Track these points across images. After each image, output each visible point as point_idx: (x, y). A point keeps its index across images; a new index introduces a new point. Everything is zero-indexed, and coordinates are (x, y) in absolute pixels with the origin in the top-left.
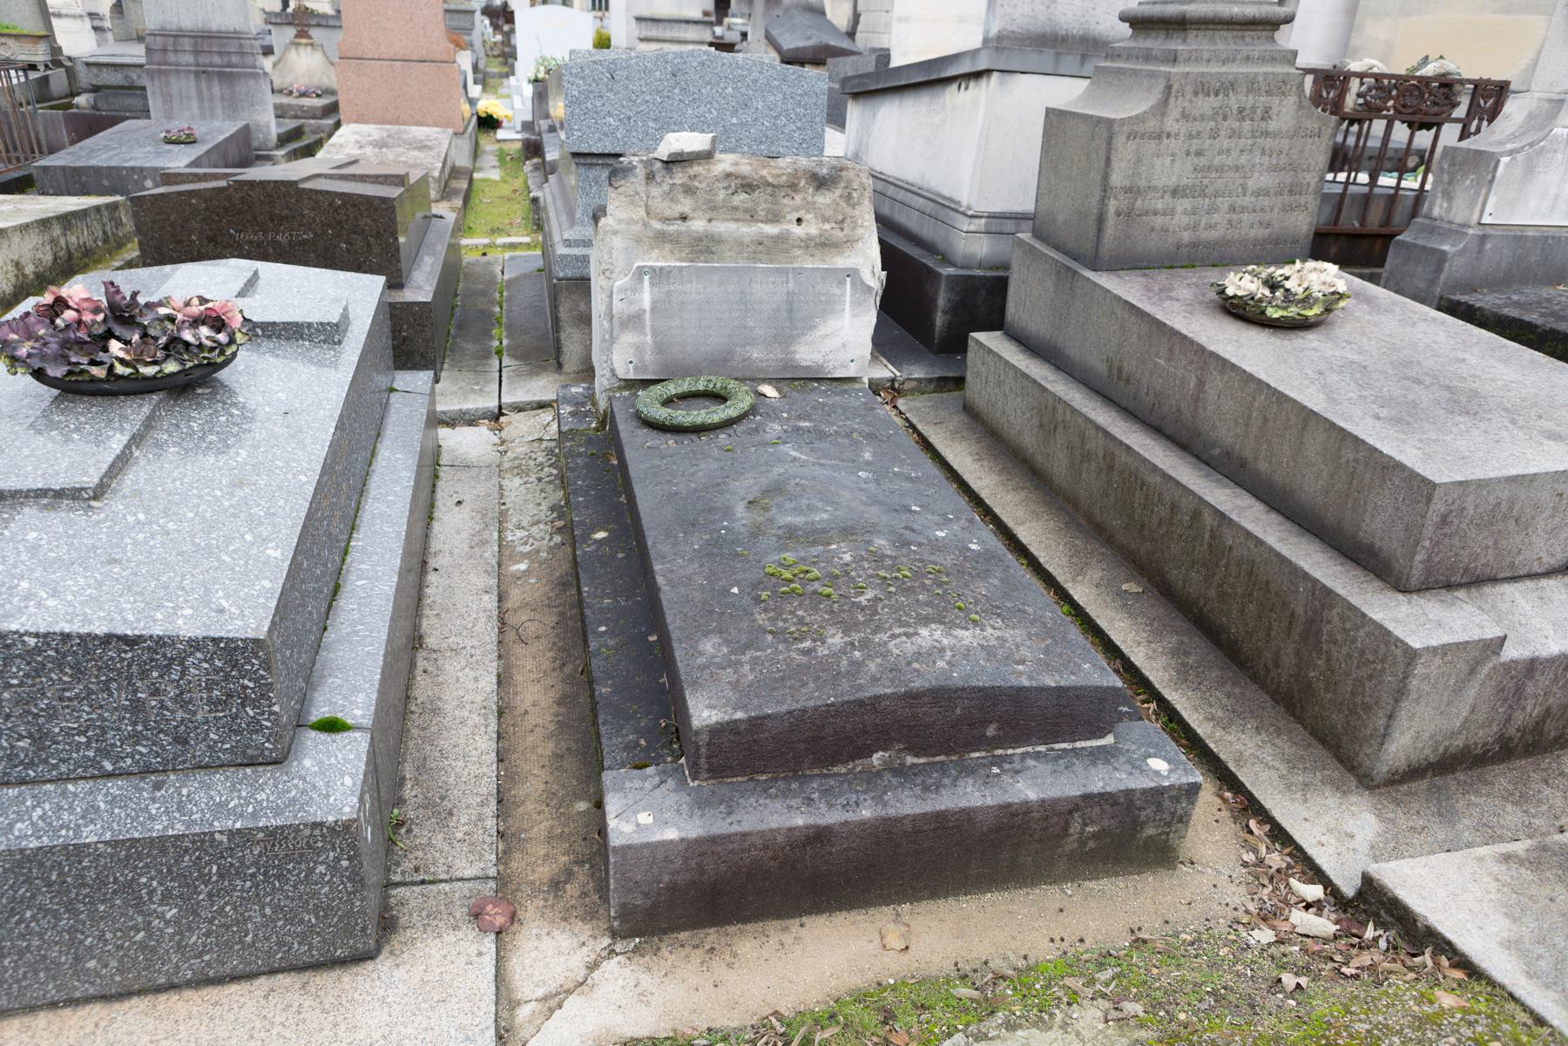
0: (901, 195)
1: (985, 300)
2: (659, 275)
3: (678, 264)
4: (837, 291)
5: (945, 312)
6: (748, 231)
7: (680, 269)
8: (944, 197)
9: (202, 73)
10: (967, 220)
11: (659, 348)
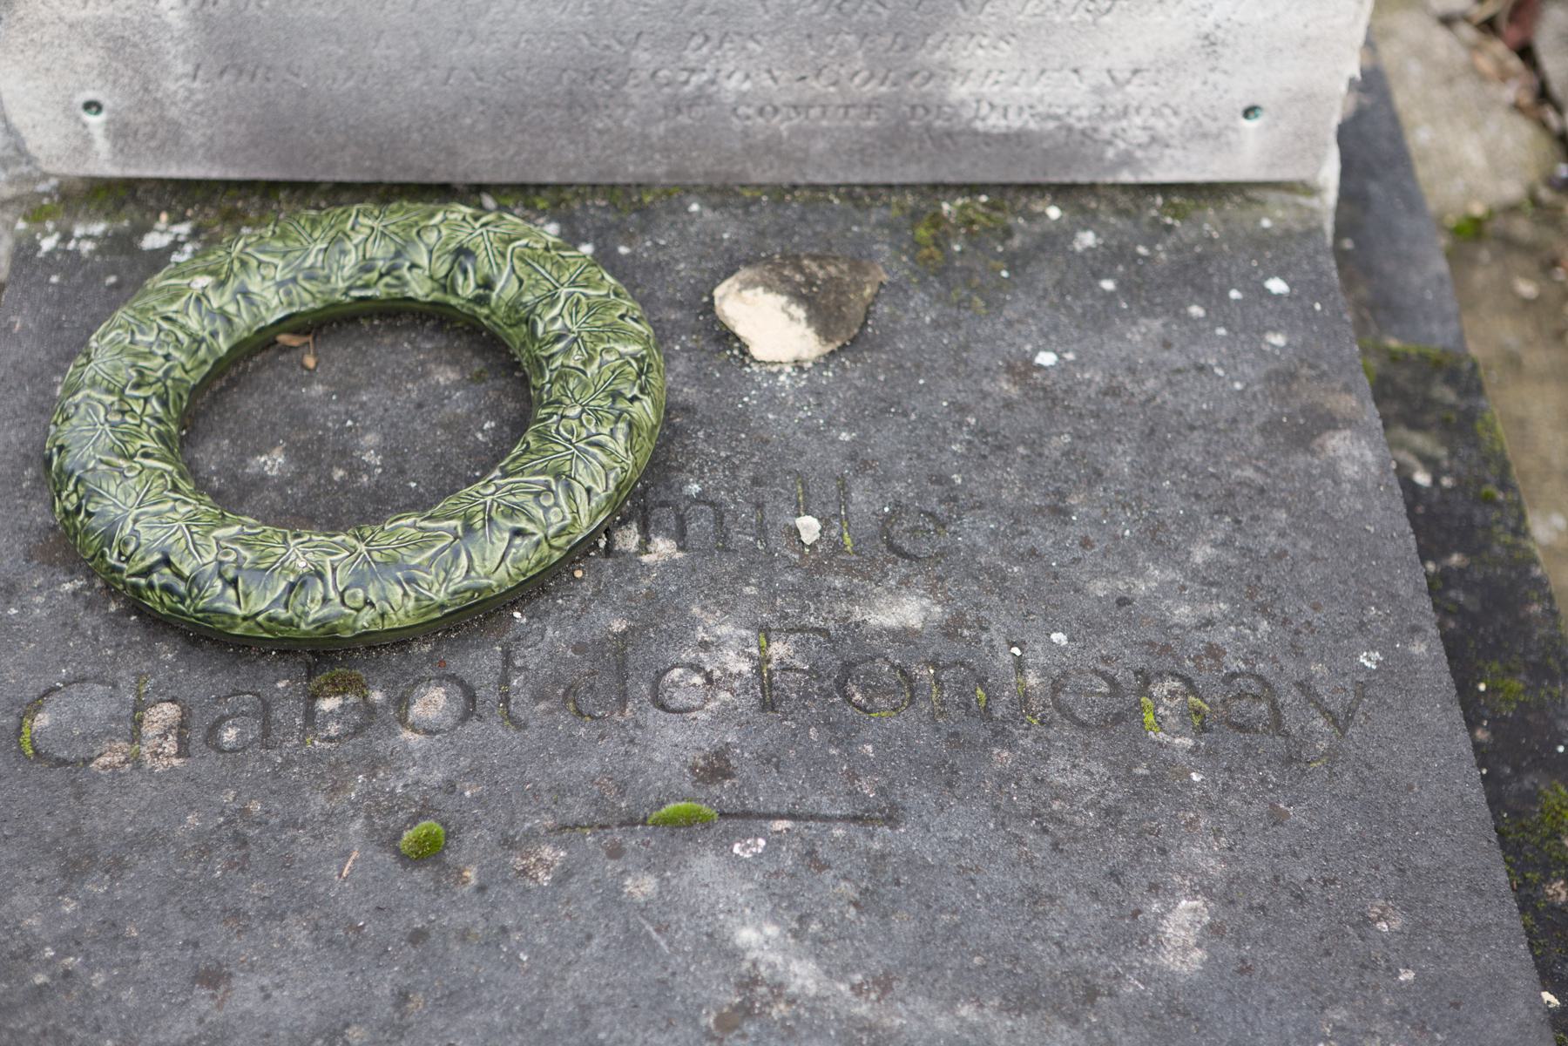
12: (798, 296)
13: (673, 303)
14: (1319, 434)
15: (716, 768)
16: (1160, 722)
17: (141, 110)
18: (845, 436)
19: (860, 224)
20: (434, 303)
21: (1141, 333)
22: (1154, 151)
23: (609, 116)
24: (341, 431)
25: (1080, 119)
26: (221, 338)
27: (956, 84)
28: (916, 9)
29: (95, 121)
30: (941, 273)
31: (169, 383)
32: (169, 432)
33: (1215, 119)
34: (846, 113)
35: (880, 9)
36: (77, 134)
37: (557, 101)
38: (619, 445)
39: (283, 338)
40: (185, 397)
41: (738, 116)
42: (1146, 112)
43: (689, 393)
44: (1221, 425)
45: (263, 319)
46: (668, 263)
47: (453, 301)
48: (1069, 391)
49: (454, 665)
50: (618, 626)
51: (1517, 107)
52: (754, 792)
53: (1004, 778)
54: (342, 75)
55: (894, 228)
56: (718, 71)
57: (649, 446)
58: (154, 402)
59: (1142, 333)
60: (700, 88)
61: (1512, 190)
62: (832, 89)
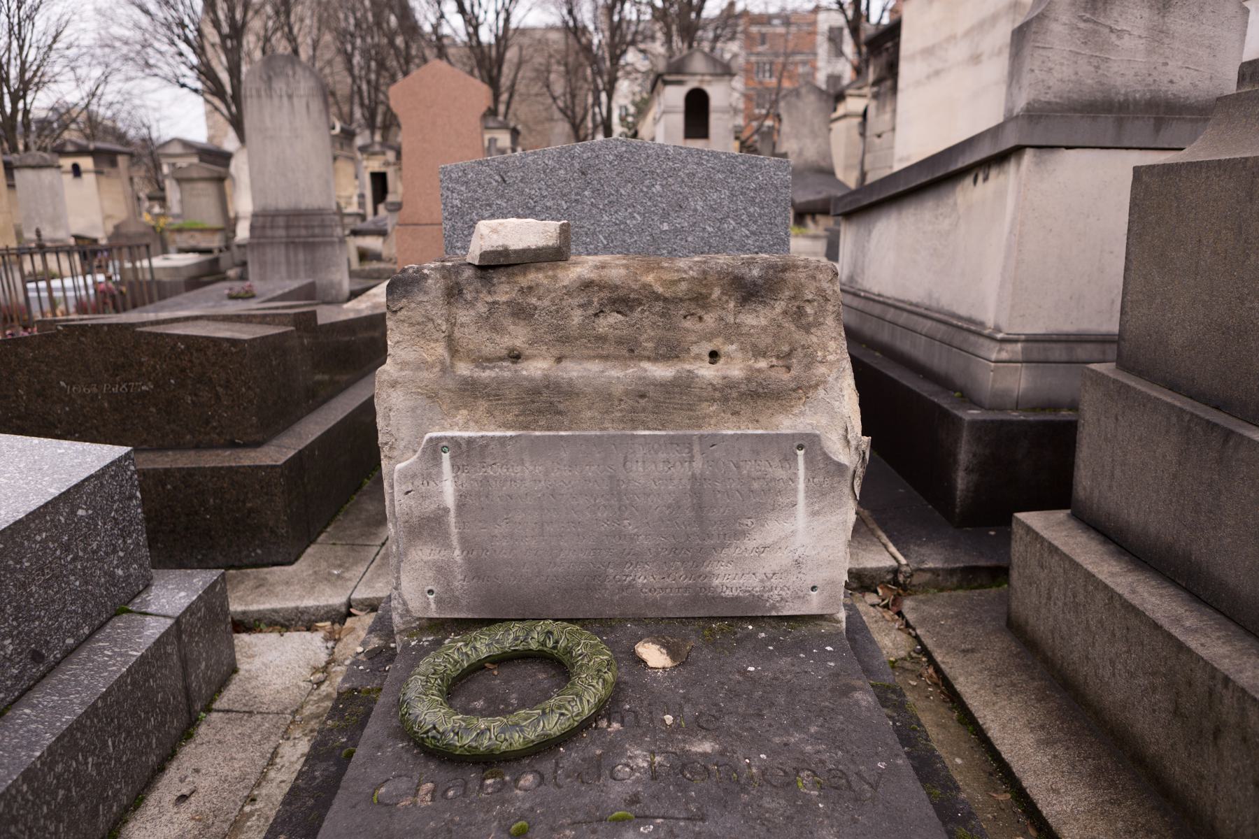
0: (903, 318)
1: (1037, 459)
2: (465, 452)
3: (498, 433)
4: (781, 473)
5: (968, 471)
6: (618, 374)
7: (502, 441)
8: (960, 318)
9: (291, 244)
10: (997, 346)
11: (476, 570)
12: (663, 646)
13: (621, 652)
15: (634, 800)
16: (805, 786)
22: (783, 604)
29: (431, 597)
38: (600, 687)
49: (537, 767)
50: (598, 752)
52: (649, 808)
53: (746, 805)
59: (784, 662)
61: (903, 654)
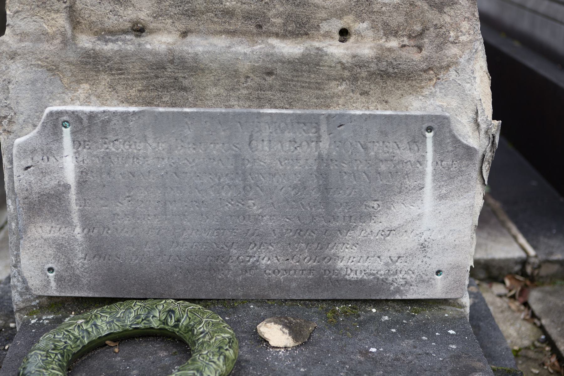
12: (285, 326)
14: (471, 373)
17: (67, 271)
18: (302, 370)
19: (308, 312)
20: (160, 329)
21: (406, 344)
22: (407, 287)
23: (223, 274)
24: (125, 370)
25: (381, 275)
26: (85, 339)
27: (339, 262)
28: (325, 234)
29: (51, 275)
30: (336, 326)
31: (65, 350)
32: (63, 365)
33: (427, 275)
34: (303, 273)
35: (313, 234)
36: (45, 280)
37: (206, 268)
38: (221, 363)
39: (107, 342)
40: (71, 356)
41: (266, 274)
42: (403, 272)
43: (248, 356)
44: (436, 370)
45: (101, 334)
46: (242, 321)
47: (167, 327)
48: (381, 359)
51: (525, 319)
54: (134, 258)
55: (320, 313)
56: (259, 257)
57: (231, 365)
58: (59, 355)
60: (253, 263)
61: (526, 343)
62: (297, 264)
